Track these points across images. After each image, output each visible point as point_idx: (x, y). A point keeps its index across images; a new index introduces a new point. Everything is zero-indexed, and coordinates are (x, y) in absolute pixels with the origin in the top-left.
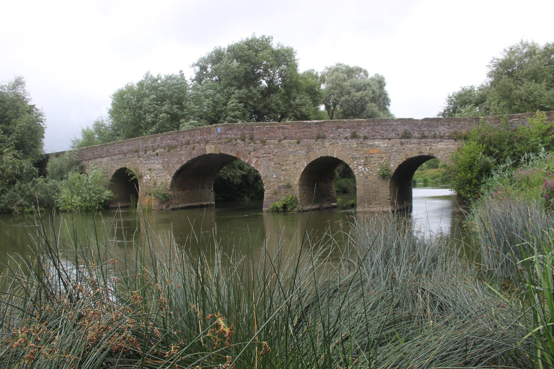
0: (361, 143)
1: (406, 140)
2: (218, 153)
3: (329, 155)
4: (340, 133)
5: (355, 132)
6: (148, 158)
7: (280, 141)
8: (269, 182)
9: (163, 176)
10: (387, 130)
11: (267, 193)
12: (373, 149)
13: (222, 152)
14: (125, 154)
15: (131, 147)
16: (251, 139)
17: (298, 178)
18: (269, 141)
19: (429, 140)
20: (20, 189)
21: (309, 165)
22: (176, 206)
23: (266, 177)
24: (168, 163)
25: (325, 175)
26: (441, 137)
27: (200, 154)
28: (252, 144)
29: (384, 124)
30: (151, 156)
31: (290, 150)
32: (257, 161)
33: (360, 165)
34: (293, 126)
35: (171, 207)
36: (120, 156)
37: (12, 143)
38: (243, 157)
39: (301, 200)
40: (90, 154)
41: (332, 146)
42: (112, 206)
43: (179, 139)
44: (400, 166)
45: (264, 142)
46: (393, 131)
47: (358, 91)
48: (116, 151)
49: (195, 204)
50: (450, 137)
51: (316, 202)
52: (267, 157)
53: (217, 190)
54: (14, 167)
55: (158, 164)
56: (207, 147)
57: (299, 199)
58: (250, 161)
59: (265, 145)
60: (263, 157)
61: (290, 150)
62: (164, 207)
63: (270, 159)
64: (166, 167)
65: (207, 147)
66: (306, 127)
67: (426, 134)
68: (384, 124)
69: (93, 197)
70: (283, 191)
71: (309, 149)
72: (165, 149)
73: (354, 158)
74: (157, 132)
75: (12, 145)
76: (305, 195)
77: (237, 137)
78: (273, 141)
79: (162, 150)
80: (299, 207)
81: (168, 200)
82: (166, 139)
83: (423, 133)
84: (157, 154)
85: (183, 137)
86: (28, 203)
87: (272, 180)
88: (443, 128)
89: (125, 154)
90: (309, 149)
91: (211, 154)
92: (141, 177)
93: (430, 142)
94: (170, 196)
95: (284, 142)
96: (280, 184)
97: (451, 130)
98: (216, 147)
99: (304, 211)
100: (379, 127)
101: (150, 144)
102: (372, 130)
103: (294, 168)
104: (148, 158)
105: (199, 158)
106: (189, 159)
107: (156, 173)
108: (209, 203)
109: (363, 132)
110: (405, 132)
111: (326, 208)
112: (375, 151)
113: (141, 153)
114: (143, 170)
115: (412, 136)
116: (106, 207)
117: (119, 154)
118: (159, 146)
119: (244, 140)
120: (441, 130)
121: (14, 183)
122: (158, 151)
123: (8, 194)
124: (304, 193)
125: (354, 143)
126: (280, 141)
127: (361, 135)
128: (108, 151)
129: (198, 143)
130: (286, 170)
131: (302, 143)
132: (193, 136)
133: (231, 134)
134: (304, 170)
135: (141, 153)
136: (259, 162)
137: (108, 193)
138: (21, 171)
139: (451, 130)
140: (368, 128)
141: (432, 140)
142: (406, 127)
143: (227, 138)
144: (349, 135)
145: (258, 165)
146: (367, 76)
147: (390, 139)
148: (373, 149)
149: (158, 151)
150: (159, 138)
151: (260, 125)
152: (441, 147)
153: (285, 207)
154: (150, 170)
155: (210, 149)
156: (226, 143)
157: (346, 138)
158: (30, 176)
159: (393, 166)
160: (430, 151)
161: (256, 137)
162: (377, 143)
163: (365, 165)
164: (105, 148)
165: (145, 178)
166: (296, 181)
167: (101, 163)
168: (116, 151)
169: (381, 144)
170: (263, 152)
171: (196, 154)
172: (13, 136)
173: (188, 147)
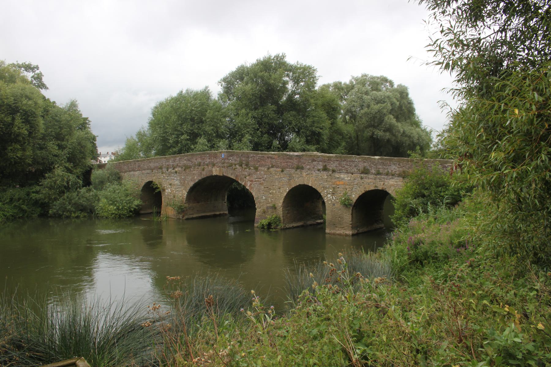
0: (330, 175)
1: (365, 175)
2: (222, 175)
3: (306, 183)
4: (315, 166)
5: (326, 166)
6: (169, 175)
7: (268, 169)
8: (260, 203)
9: (180, 191)
10: (351, 166)
11: (258, 211)
12: (339, 181)
13: (225, 174)
14: (152, 170)
15: (156, 164)
16: (247, 165)
17: (282, 201)
18: (260, 168)
19: (383, 176)
20: (68, 197)
21: (290, 191)
22: (191, 216)
23: (258, 198)
24: (184, 180)
25: (304, 200)
26: (393, 175)
27: (208, 175)
28: (248, 170)
29: (349, 160)
30: (172, 173)
31: (276, 177)
32: (251, 184)
33: (329, 193)
34: (279, 157)
35: (186, 217)
36: (149, 171)
37: (65, 157)
38: (241, 180)
39: (284, 220)
40: (126, 168)
41: (308, 176)
42: (142, 212)
43: (193, 160)
44: (360, 197)
45: (256, 169)
46: (355, 166)
47: (377, 103)
48: (145, 166)
49: (208, 214)
50: (399, 175)
51: (300, 220)
52: (258, 181)
53: (231, 200)
54: (63, 180)
55: (177, 180)
56: (214, 169)
57: (282, 219)
58: (245, 183)
59: (257, 171)
60: (255, 181)
61: (276, 177)
62: (181, 216)
63: (261, 184)
64: (183, 184)
65: (214, 169)
66: (288, 158)
67: (381, 171)
68: (349, 160)
69: (125, 206)
70: (270, 211)
71: (291, 177)
72: (182, 168)
73: (325, 188)
74: (180, 152)
75: (65, 159)
76: (289, 215)
77: (236, 163)
78: (263, 168)
79: (180, 169)
80: (282, 225)
81: (184, 211)
82: (183, 160)
83: (379, 171)
84: (176, 172)
85: (196, 160)
86: (74, 210)
87: (262, 201)
88: (394, 167)
89: (152, 170)
90: (291, 177)
91: (216, 176)
92: (164, 190)
93: (384, 178)
94: (186, 207)
95: (272, 169)
96: (268, 205)
97: (401, 169)
98: (220, 170)
99: (287, 229)
100: (344, 163)
101: (171, 163)
102: (339, 164)
103: (279, 192)
104: (169, 175)
105: (208, 178)
106: (200, 178)
107: (175, 188)
108: (222, 213)
109: (332, 166)
110: (364, 168)
111: (311, 225)
112: (341, 183)
113: (164, 170)
114: (165, 185)
115: (369, 172)
116: (135, 215)
117: (148, 169)
118: (177, 165)
119: (241, 166)
120: (392, 169)
121: (64, 192)
122: (177, 169)
123: (59, 202)
124: (288, 213)
125: (325, 175)
126: (268, 169)
127: (331, 168)
128: (139, 166)
129: (207, 165)
130: (272, 193)
131: (285, 172)
132: (204, 159)
133: (232, 160)
134: (287, 195)
135: (164, 170)
136: (252, 186)
137: (137, 202)
138: (68, 183)
139: (401, 169)
140: (336, 163)
141: (386, 177)
142: (365, 164)
143: (228, 163)
144: (321, 167)
145: (252, 188)
146: (392, 86)
147: (352, 174)
148: (339, 181)
149: (177, 169)
150: (178, 158)
151: (254, 154)
152: (392, 183)
153: (269, 225)
154: (171, 184)
155: (216, 172)
156: (228, 167)
157: (319, 170)
158: (76, 187)
159: (354, 197)
160: (384, 186)
161: (251, 163)
162: (342, 176)
163: (333, 194)
164: (137, 163)
165: (167, 191)
166: (280, 203)
167: (134, 175)
168: (145, 166)
169: (346, 177)
170: (256, 177)
171: (205, 174)
172: (66, 151)
173: (200, 168)
